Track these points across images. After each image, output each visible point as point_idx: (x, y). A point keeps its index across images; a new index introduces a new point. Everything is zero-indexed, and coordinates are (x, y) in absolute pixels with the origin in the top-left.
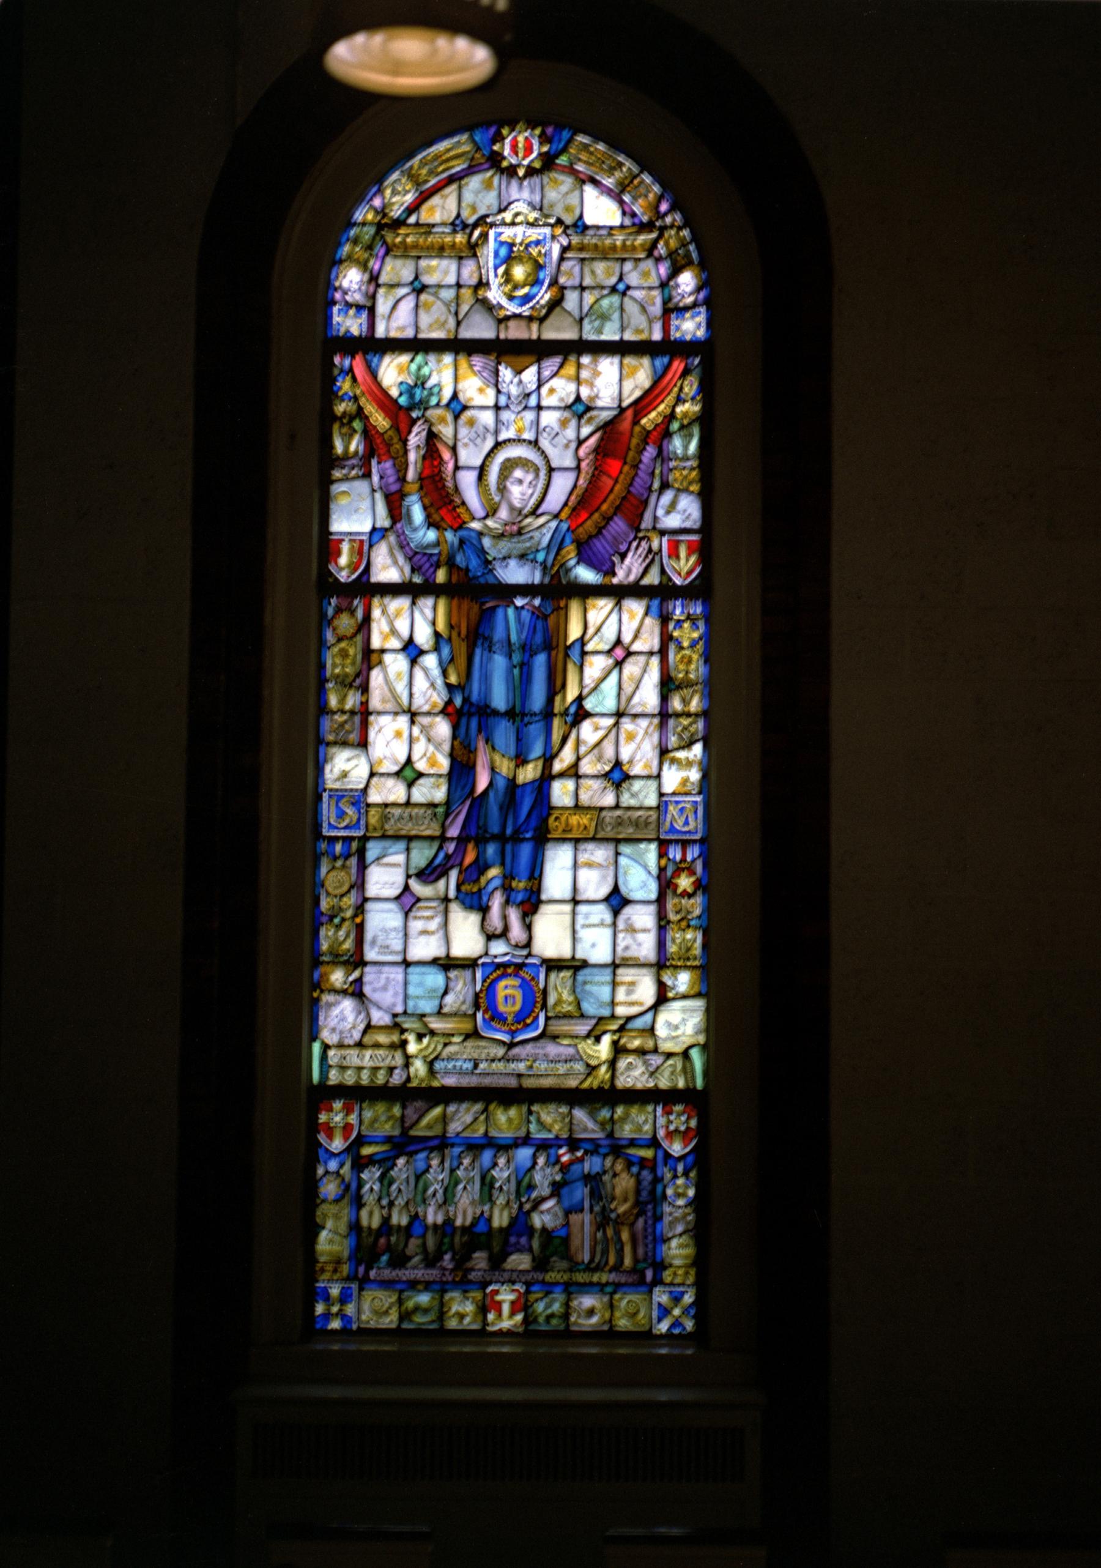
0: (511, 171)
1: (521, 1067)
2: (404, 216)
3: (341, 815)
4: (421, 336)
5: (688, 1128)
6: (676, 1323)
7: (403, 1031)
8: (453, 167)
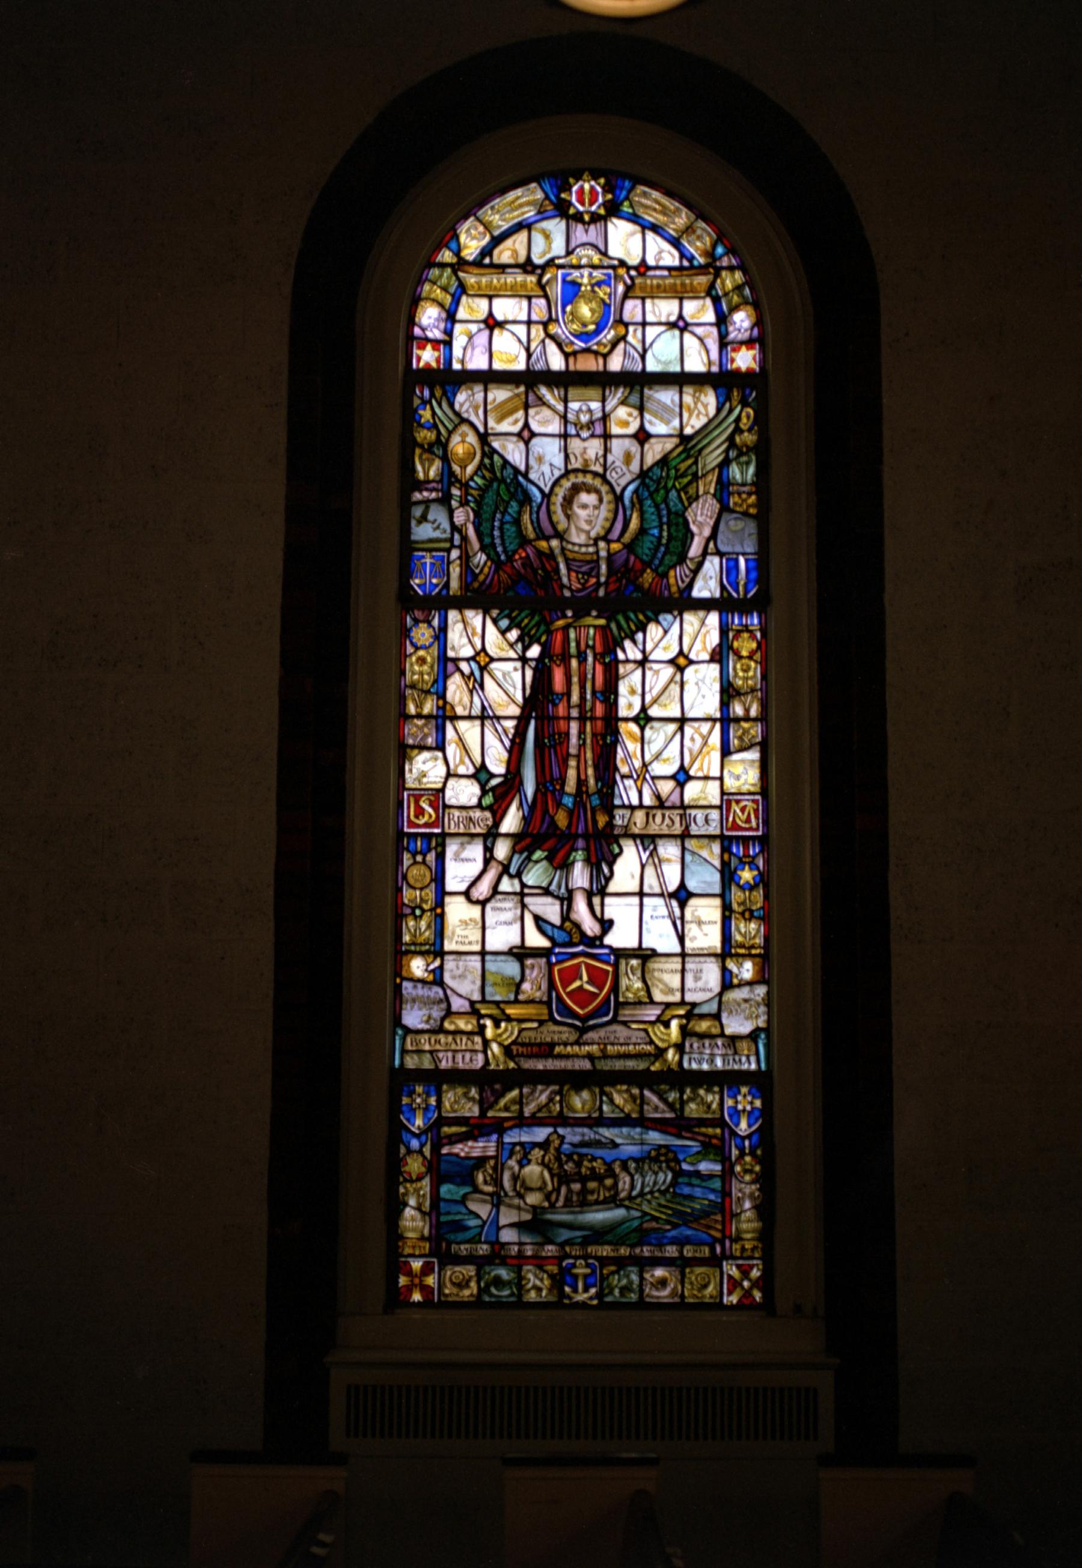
0: (578, 218)
1: (594, 1049)
2: (479, 258)
3: (420, 812)
5: (753, 1109)
6: (748, 1294)
7: (481, 1016)
8: (523, 213)
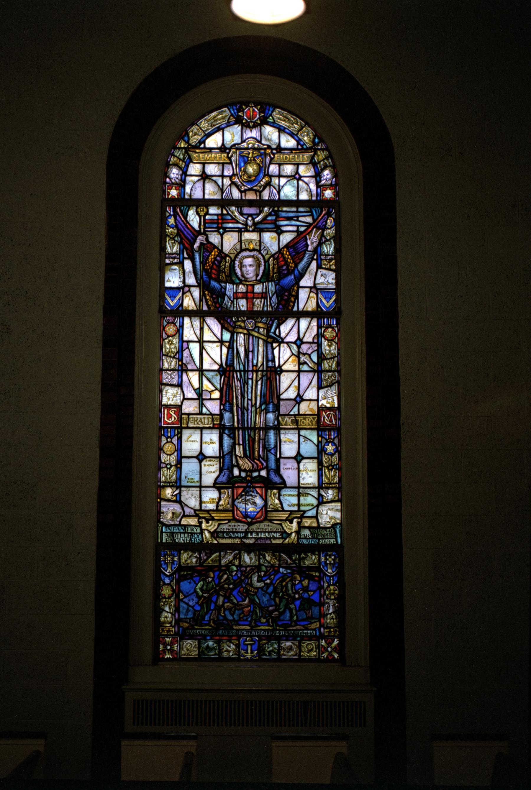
4: (207, 197)
